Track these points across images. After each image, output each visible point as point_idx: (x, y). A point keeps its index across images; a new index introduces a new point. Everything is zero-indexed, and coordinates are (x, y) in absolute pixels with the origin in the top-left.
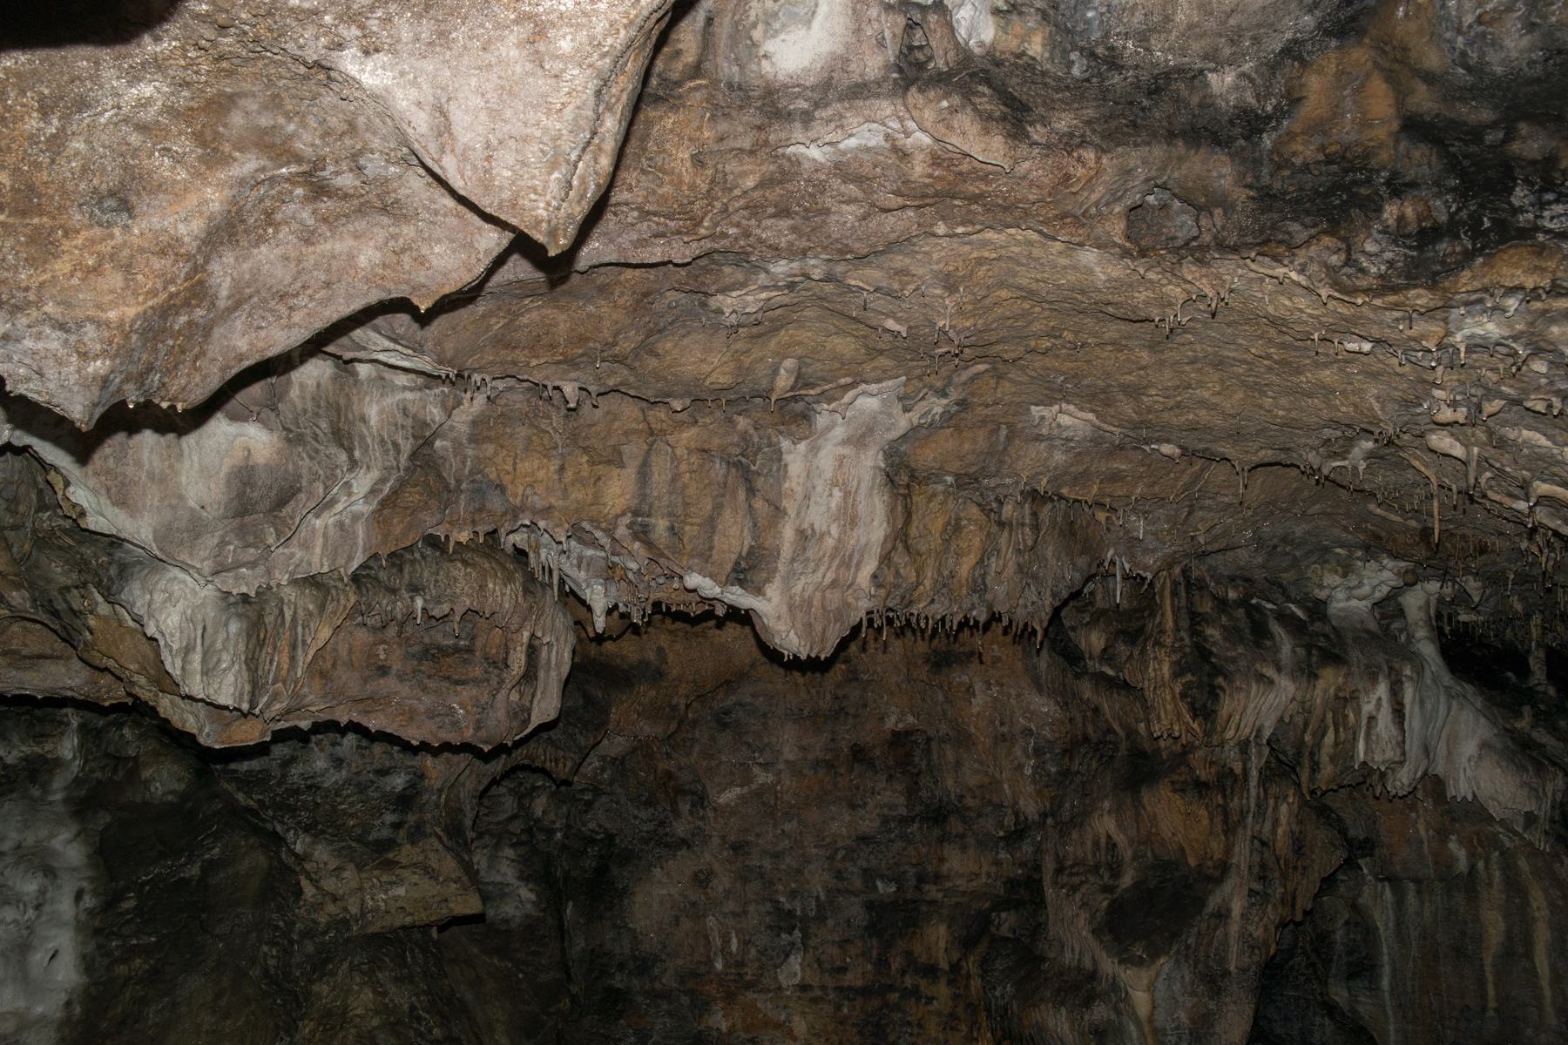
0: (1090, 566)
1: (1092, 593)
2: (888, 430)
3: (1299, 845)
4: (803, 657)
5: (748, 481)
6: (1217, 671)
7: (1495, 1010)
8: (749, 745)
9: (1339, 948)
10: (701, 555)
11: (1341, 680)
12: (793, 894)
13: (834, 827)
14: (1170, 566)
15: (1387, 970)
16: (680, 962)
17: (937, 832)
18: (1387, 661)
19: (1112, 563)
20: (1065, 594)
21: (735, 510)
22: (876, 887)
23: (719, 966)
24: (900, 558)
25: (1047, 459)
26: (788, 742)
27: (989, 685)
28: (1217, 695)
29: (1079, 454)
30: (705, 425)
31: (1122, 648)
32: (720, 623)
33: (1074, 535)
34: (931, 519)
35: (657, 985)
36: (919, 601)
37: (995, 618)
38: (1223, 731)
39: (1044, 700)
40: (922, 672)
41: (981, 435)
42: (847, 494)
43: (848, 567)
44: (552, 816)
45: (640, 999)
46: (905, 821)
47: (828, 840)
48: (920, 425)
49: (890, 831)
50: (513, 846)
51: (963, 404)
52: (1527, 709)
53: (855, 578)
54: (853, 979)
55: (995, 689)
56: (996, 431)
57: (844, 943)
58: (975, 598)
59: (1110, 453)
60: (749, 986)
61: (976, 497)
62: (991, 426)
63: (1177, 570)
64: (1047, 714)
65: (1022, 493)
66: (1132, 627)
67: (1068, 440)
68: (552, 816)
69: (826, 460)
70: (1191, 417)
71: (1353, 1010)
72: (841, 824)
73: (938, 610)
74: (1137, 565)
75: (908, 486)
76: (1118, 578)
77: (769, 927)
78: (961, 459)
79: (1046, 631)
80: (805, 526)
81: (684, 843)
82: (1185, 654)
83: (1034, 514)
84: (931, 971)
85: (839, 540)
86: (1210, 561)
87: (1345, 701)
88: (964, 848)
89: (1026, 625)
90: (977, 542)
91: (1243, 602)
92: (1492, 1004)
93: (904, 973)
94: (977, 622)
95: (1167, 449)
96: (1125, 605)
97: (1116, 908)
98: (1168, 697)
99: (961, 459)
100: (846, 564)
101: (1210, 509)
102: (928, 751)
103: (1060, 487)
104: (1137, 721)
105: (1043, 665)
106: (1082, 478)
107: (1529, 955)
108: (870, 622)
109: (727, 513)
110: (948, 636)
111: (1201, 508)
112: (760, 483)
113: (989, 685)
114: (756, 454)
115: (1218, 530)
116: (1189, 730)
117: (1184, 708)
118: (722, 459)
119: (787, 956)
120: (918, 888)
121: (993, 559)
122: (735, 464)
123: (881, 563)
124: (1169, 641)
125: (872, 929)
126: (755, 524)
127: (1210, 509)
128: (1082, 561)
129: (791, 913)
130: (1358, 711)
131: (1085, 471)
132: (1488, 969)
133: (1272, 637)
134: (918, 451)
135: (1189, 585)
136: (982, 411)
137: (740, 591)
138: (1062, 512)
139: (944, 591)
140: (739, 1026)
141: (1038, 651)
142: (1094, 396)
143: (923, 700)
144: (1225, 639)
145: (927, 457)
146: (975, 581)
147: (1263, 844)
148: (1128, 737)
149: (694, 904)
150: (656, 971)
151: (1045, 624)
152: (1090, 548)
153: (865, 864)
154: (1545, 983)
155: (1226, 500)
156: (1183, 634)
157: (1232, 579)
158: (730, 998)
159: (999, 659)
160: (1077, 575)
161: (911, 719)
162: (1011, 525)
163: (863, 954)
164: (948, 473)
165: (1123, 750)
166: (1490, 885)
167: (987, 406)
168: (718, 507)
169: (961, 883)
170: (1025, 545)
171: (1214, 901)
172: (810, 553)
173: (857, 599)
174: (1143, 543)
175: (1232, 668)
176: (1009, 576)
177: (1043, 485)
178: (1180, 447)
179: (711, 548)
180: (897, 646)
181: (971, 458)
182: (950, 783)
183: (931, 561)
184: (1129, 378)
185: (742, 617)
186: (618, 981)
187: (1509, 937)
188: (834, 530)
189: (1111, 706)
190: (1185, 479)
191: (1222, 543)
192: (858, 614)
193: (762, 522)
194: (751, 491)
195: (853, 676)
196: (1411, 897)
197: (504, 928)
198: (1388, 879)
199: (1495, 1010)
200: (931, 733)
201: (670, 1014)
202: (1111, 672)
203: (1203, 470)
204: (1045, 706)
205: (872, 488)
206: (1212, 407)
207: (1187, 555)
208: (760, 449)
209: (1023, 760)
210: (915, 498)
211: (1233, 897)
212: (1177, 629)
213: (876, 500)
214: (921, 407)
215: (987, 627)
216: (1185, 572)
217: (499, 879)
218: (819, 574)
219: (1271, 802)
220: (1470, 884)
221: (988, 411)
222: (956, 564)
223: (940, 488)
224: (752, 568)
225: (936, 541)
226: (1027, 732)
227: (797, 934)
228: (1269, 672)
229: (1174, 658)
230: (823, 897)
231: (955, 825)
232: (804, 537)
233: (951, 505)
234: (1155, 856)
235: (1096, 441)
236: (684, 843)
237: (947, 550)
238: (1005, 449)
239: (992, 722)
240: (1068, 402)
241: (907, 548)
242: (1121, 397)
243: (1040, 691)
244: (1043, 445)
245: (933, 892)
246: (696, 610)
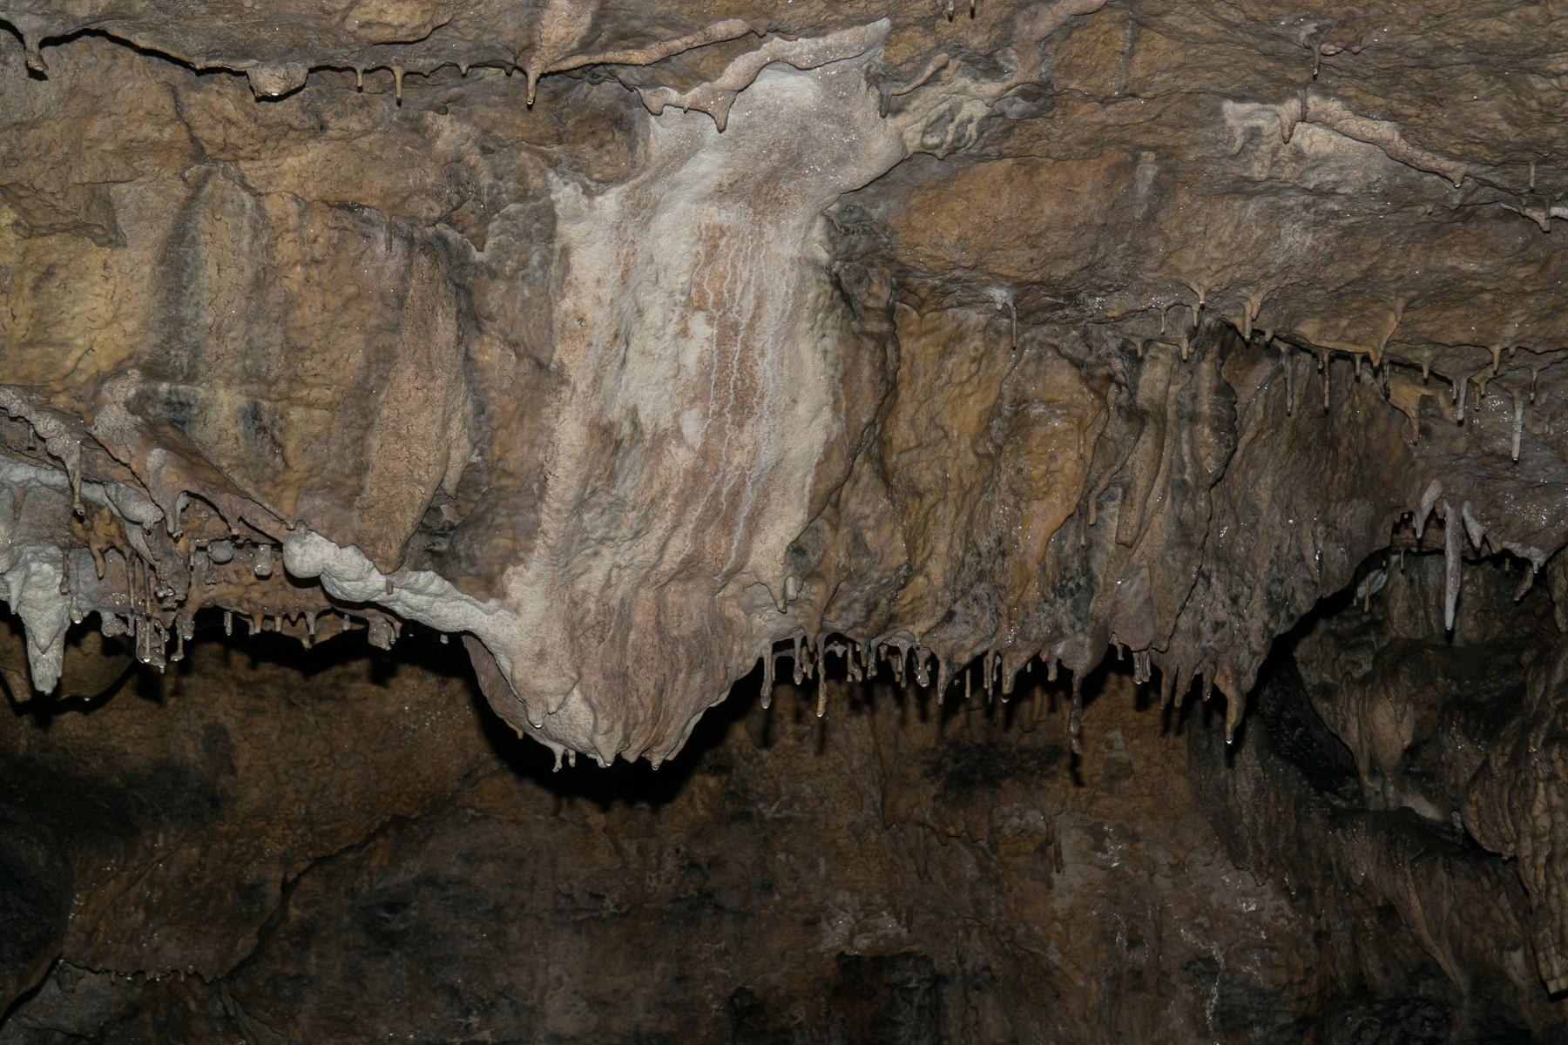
0: (1372, 528)
19: (1436, 520)
29: (1350, 231)
33: (1332, 444)
131: (1366, 276)
184: (1492, 23)
189: (1428, 902)
202: (1429, 811)
235: (1399, 197)
242: (1471, 78)
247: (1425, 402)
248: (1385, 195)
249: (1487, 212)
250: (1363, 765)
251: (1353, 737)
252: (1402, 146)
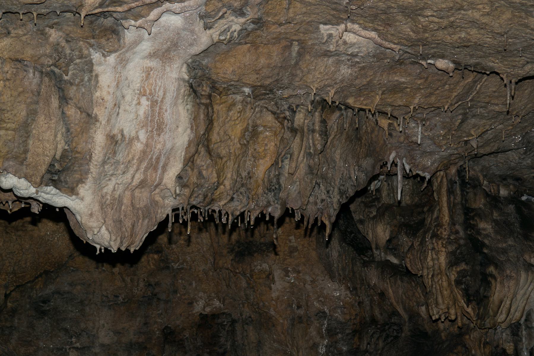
0: (374, 167)
1: (378, 190)
2: (191, 45)
4: (114, 250)
5: (61, 89)
6: (489, 261)
8: (66, 330)
10: (16, 158)
14: (446, 167)
19: (394, 164)
20: (351, 192)
21: (48, 116)
24: (203, 161)
25: (334, 73)
27: (287, 273)
28: (489, 284)
29: (363, 68)
30: (18, 37)
31: (405, 240)
32: (36, 219)
33: (360, 139)
34: (231, 126)
36: (220, 199)
37: (288, 213)
38: (496, 314)
39: (336, 285)
40: (227, 261)
41: (276, 50)
42: (154, 103)
43: (155, 169)
48: (220, 42)
51: (258, 22)
53: (161, 179)
55: (292, 275)
56: (288, 47)
58: (271, 196)
59: (391, 67)
61: (271, 106)
62: (284, 43)
63: (453, 170)
64: (339, 298)
65: (312, 102)
66: (414, 220)
67: (353, 55)
69: (134, 71)
70: (463, 35)
73: (237, 207)
74: (416, 166)
75: (210, 96)
76: (400, 177)
78: (257, 72)
79: (334, 225)
80: (115, 131)
82: (460, 246)
83: (324, 122)
85: (147, 145)
86: (484, 162)
89: (316, 220)
90: (271, 146)
91: (514, 199)
94: (272, 218)
95: (441, 64)
96: (407, 201)
98: (445, 284)
99: (257, 72)
100: (153, 166)
101: (482, 117)
102: (233, 332)
103: (346, 97)
104: (419, 305)
105: (335, 254)
106: (366, 90)
108: (177, 217)
109: (41, 119)
110: (246, 230)
111: (474, 116)
112: (72, 91)
113: (287, 273)
114: (68, 65)
115: (489, 135)
116: (464, 314)
117: (459, 294)
118: (35, 68)
121: (287, 162)
122: (48, 74)
123: (185, 165)
124: (445, 234)
126: (68, 130)
127: (482, 117)
128: (367, 163)
131: (369, 83)
134: (218, 65)
135: (463, 184)
136: (275, 29)
137: (54, 191)
138: (350, 120)
139: (243, 190)
141: (328, 242)
142: (376, 16)
143: (228, 286)
144: (496, 232)
145: (226, 70)
146: (270, 181)
148: (411, 318)
151: (333, 219)
152: (374, 151)
155: (497, 108)
156: (458, 227)
157: (504, 178)
159: (295, 249)
160: (362, 176)
161: (217, 303)
162: (303, 131)
164: (246, 85)
165: (406, 331)
167: (281, 25)
168: (33, 113)
170: (315, 150)
172: (120, 157)
173: (164, 198)
174: (422, 146)
175: (502, 258)
176: (305, 178)
177: (330, 96)
178: (454, 62)
179: (26, 151)
180: (205, 238)
181: (266, 72)
183: (230, 164)
185: (59, 215)
188: (143, 136)
189: (395, 291)
190: (459, 90)
191: (494, 147)
192: (165, 210)
193: (74, 128)
194: (64, 99)
195: (165, 265)
200: (235, 316)
202: (395, 261)
203: (475, 82)
204: (337, 291)
205: (177, 98)
206: (482, 27)
207: (462, 157)
208: (71, 60)
209: (318, 340)
210: (216, 107)
212: (453, 223)
213: (181, 108)
214: (221, 25)
215: (281, 222)
216: (460, 172)
218: (129, 176)
221: (282, 29)
222: (253, 166)
223: (239, 98)
224: (65, 170)
225: (235, 145)
226: (321, 315)
229: (451, 248)
232: (113, 141)
233: (248, 113)
235: (379, 57)
237: (245, 154)
238: (297, 64)
239: (290, 306)
240: (353, 22)
241: (209, 152)
242: (400, 17)
243: (332, 277)
244: (331, 60)
246: (13, 207)
247: (390, 125)
248: (374, 56)
249: (407, 62)
250: (374, 246)
251: (370, 237)
252: (379, 40)
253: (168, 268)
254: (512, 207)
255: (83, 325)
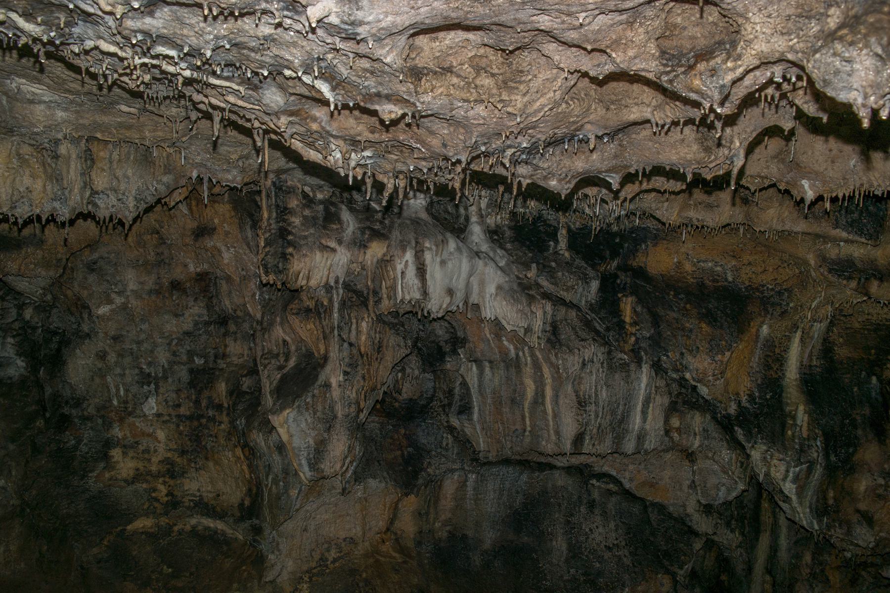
3: (379, 348)
7: (530, 432)
8: (108, 281)
9: (457, 397)
11: (385, 249)
12: (150, 364)
13: (168, 327)
15: (476, 409)
16: (98, 400)
17: (223, 330)
18: (416, 239)
22: (194, 361)
23: (115, 402)
26: (131, 280)
35: (85, 413)
44: (36, 319)
45: (76, 420)
46: (207, 324)
47: (166, 334)
49: (199, 329)
50: (14, 337)
52: (534, 265)
54: (183, 411)
57: (178, 391)
60: (130, 414)
68: (36, 319)
71: (463, 431)
72: (171, 326)
77: (137, 382)
81: (88, 335)
84: (219, 407)
87: (385, 263)
88: (235, 340)
92: (529, 429)
93: (207, 408)
97: (283, 380)
107: (543, 404)
119: (147, 398)
120: (215, 362)
125: (192, 384)
129: (149, 375)
130: (394, 269)
132: (526, 410)
133: (340, 221)
140: (129, 435)
147: (351, 345)
149: (100, 369)
150: (85, 405)
153: (189, 348)
154: (550, 418)
158: (121, 420)
163: (188, 397)
166: (526, 364)
169: (235, 360)
171: (322, 378)
182: (227, 303)
186: (66, 410)
187: (536, 394)
196: (487, 370)
197: (9, 382)
198: (475, 361)
199: (530, 432)
201: (91, 428)
211: (333, 374)
217: (7, 355)
219: (354, 321)
220: (515, 365)
227: (153, 386)
228: (333, 244)
230: (166, 366)
231: (232, 327)
234: (307, 350)
236: (88, 335)
245: (222, 364)
253: (165, 243)
254: (321, 207)
255: (118, 278)
